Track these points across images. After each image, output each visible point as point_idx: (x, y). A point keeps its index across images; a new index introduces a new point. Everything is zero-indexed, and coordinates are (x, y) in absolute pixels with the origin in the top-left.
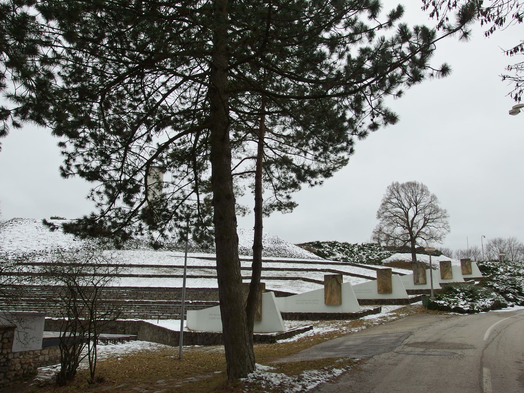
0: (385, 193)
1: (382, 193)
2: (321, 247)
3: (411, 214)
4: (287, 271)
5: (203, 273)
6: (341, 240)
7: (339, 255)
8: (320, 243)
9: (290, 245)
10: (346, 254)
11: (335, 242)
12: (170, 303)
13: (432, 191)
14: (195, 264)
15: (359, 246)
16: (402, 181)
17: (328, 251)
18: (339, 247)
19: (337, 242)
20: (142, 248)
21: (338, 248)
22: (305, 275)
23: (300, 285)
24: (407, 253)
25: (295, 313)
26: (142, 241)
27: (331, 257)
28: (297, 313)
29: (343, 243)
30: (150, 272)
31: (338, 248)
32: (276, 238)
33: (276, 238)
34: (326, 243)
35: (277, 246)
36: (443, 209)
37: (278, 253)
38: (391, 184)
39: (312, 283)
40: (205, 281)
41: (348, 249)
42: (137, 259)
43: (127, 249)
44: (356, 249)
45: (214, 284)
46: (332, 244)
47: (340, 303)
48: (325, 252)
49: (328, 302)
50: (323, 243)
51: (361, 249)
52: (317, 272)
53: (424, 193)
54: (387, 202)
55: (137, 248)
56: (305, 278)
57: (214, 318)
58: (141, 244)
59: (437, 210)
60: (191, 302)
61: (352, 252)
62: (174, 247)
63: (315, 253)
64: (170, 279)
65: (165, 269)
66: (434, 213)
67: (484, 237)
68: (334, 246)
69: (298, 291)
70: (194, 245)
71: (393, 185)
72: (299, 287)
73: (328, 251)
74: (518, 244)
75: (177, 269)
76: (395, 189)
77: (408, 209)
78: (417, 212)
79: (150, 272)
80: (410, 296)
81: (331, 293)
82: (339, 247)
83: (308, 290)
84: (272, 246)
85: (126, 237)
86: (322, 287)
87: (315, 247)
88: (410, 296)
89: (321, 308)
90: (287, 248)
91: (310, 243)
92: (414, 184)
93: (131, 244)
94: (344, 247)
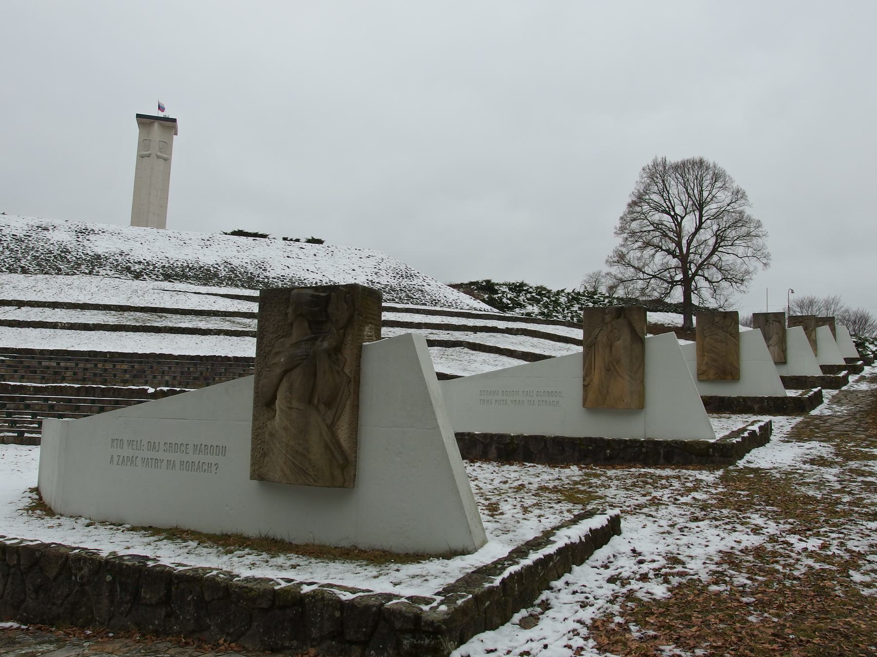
0: (638, 179)
1: (631, 183)
2: (496, 292)
3: (689, 224)
4: (430, 331)
5: (226, 326)
6: (533, 282)
7: (535, 309)
8: (493, 284)
9: (431, 283)
10: (546, 307)
11: (522, 285)
12: (88, 391)
13: (739, 180)
14: (215, 308)
15: (569, 294)
16: (674, 158)
17: (510, 299)
18: (531, 293)
19: (526, 285)
20: (102, 272)
21: (529, 296)
22: (472, 337)
23: (467, 358)
24: (661, 311)
25: (485, 436)
26: (107, 258)
27: (517, 310)
28: (491, 436)
29: (537, 288)
30: (111, 319)
31: (529, 296)
32: (403, 267)
33: (403, 267)
34: (505, 285)
35: (405, 282)
36: (755, 217)
37: (407, 296)
38: (651, 164)
39: (492, 355)
40: (225, 342)
41: (549, 298)
42: (77, 292)
43: (67, 274)
44: (563, 300)
45: (247, 348)
46: (516, 286)
47: (639, 404)
48: (505, 300)
49: (596, 399)
50: (497, 284)
51: (573, 298)
52: (499, 335)
53: (718, 184)
54: (639, 199)
55: (90, 273)
56: (474, 344)
57: (132, 461)
58: (101, 265)
59: (740, 221)
60: (151, 390)
61: (556, 303)
62: (177, 275)
63: (484, 301)
64: (145, 335)
65: (139, 314)
66: (736, 227)
67: (793, 292)
68: (520, 291)
69: (465, 370)
70: (224, 273)
71: (655, 165)
72: (466, 363)
73: (510, 299)
74: (843, 309)
75: (169, 315)
76: (659, 173)
77: (682, 218)
78: (701, 223)
79: (111, 319)
80: (791, 393)
81: (610, 370)
82: (531, 293)
83: (488, 369)
84: (394, 283)
85: (668, 559)
86: (580, 349)
87: (484, 289)
88: (791, 393)
89: (571, 420)
90: (427, 288)
91: (472, 283)
92: (701, 164)
93: (79, 265)
94: (539, 294)
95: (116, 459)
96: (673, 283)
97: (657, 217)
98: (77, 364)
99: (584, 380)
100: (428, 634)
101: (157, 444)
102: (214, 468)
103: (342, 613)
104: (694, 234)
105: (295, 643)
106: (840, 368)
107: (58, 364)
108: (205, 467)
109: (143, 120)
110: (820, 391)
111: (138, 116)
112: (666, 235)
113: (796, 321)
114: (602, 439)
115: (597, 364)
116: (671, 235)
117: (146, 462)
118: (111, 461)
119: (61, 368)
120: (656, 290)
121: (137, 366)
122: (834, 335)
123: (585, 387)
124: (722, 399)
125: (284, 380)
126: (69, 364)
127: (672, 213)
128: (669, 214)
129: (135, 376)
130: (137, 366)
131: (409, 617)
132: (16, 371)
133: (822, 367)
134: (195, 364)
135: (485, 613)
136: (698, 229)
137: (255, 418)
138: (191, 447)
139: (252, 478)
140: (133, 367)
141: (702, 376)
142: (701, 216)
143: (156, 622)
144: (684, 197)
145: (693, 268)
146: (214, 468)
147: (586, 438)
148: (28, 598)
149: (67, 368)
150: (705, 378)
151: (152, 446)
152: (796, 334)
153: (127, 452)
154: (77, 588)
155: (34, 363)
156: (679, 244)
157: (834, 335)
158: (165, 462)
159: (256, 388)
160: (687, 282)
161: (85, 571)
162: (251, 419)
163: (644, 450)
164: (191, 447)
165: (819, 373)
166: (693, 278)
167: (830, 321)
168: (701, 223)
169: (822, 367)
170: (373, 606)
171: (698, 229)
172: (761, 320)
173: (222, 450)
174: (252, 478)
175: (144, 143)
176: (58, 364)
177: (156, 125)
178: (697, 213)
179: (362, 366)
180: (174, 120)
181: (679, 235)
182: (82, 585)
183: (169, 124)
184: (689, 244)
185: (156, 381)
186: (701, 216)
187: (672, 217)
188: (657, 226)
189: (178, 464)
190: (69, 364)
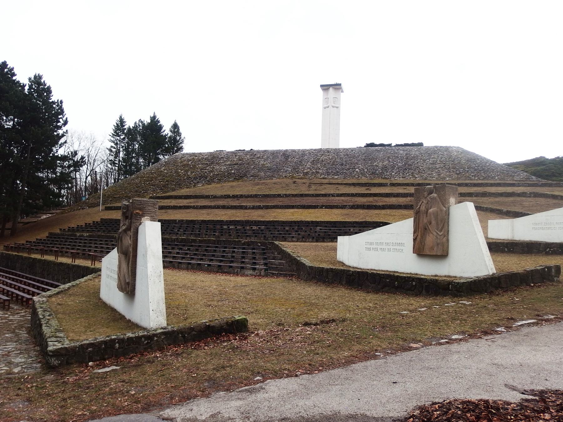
49: (420, 250)
109: (325, 88)
111: (322, 86)
123: (415, 240)
175: (326, 99)
177: (331, 89)
180: (340, 85)
183: (337, 87)
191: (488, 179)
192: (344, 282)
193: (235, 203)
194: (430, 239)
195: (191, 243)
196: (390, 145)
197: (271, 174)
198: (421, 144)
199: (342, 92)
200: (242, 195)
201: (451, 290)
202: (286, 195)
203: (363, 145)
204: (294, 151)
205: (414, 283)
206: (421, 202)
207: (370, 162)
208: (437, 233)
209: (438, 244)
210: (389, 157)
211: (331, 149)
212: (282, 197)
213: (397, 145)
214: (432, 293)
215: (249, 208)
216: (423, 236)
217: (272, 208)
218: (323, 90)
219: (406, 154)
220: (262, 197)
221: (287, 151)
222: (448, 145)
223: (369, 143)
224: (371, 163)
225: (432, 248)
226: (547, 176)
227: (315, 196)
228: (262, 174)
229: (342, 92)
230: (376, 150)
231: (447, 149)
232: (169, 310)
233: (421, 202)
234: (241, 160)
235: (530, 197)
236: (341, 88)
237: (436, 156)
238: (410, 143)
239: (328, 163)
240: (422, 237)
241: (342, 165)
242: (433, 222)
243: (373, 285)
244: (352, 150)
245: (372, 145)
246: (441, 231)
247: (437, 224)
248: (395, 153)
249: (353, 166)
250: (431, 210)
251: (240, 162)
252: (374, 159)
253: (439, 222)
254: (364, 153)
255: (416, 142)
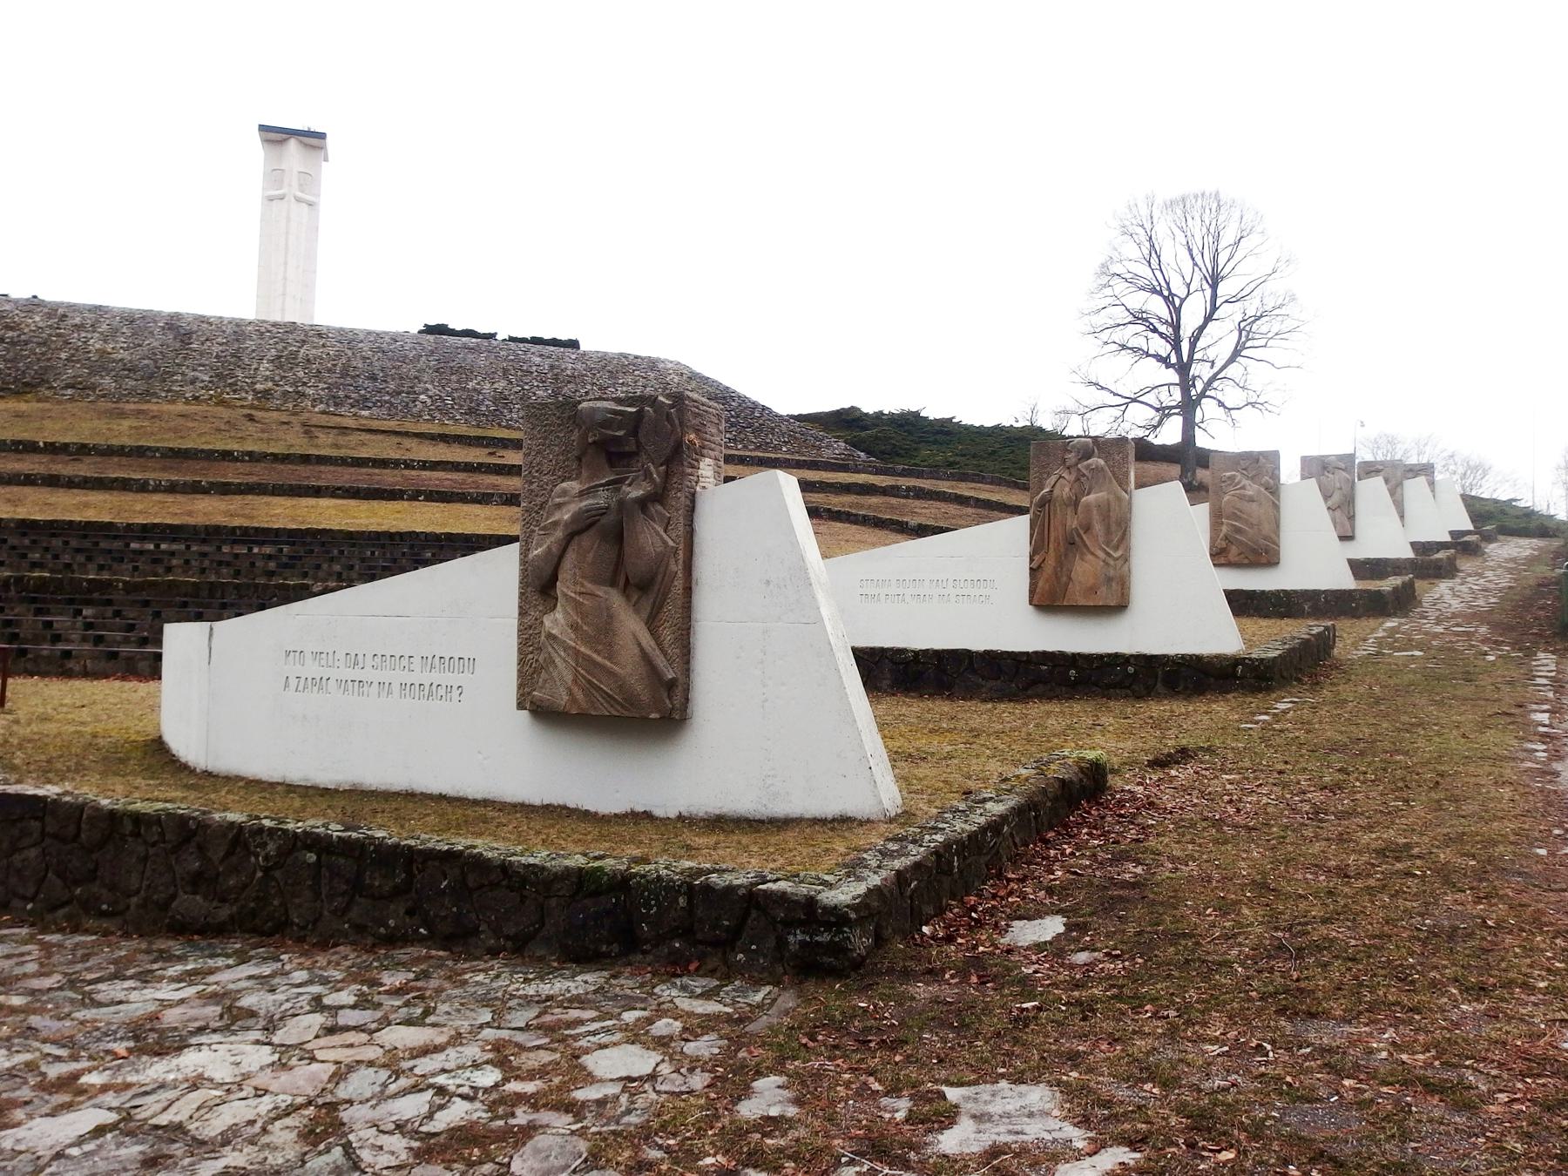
3: (1191, 317)
49: (1049, 597)
57: (319, 683)
77: (1183, 301)
95: (293, 682)
96: (1164, 412)
97: (1138, 300)
98: (188, 547)
99: (1031, 560)
100: (828, 926)
101: (360, 657)
102: (456, 692)
103: (690, 901)
104: (1202, 329)
105: (615, 948)
106: (1442, 546)
107: (157, 546)
108: (442, 691)
109: (275, 136)
110: (1409, 586)
111: (263, 128)
112: (1155, 330)
113: (1370, 470)
114: (1062, 655)
115: (1053, 535)
116: (1162, 328)
117: (343, 684)
118: (286, 686)
119: (163, 552)
120: (1135, 423)
121: (286, 549)
122: (1402, 517)
123: (1034, 572)
124: (1251, 595)
125: (570, 549)
126: (175, 547)
127: (1166, 293)
128: (1160, 293)
129: (286, 566)
130: (286, 549)
131: (797, 902)
132: (89, 559)
133: (1413, 544)
134: (383, 546)
135: (911, 898)
136: (1208, 319)
137: (523, 613)
138: (417, 661)
139: (520, 706)
140: (281, 550)
141: (1220, 556)
142: (1214, 296)
143: (392, 923)
144: (1187, 266)
145: (1199, 386)
146: (456, 692)
147: (1036, 653)
148: (181, 893)
149: (173, 554)
150: (1222, 561)
151: (355, 661)
152: (1371, 493)
153: (312, 669)
154: (259, 874)
155: (117, 545)
156: (1176, 346)
157: (1402, 517)
158: (375, 685)
159: (523, 562)
160: (1188, 407)
161: (271, 848)
162: (516, 614)
163: (1131, 669)
164: (417, 661)
165: (1410, 554)
166: (1197, 402)
167: (1426, 470)
168: (1214, 308)
169: (1413, 544)
170: (739, 886)
171: (1208, 319)
172: (1317, 468)
173: (467, 663)
174: (520, 706)
175: (275, 176)
176: (157, 546)
177: (293, 144)
178: (1208, 292)
179: (697, 526)
180: (322, 136)
181: (1176, 327)
182: (266, 870)
183: (313, 139)
184: (1193, 345)
185: (321, 574)
186: (1214, 296)
187: (1166, 299)
188: (1139, 318)
189: (396, 688)
190: (175, 547)
191: (765, 451)
192: (887, 682)
193: (84, 469)
194: (1084, 570)
195: (89, 591)
196: (492, 336)
197: (142, 386)
198: (574, 344)
199: (326, 160)
200: (84, 446)
201: (1242, 678)
202: (250, 454)
203: (415, 327)
204: (203, 320)
205: (1131, 669)
206: (1054, 478)
207: (454, 378)
208: (1108, 554)
209: (1109, 580)
210: (505, 371)
211: (328, 328)
212: (236, 460)
213: (512, 339)
214: (1186, 688)
215: (157, 489)
216: (1063, 562)
217: (241, 493)
218: (266, 141)
219: (552, 367)
220: (163, 456)
221: (177, 316)
222: (654, 355)
223: (432, 323)
224: (458, 382)
225: (1093, 590)
226: (883, 453)
227: (352, 465)
228: (107, 382)
229: (326, 160)
230: (465, 347)
231: (653, 364)
232: (128, 827)
233: (1054, 478)
234: (12, 329)
235: (907, 497)
236: (322, 148)
237: (629, 379)
238: (547, 337)
239: (329, 371)
240: (1060, 563)
241: (373, 378)
242: (1098, 527)
243: (991, 683)
244: (394, 338)
245: (440, 330)
246: (1116, 548)
247: (1108, 532)
248: (517, 359)
249: (407, 384)
250: (1092, 497)
251: (10, 334)
252: (466, 372)
253: (1113, 527)
254: (432, 352)
255: (563, 337)
